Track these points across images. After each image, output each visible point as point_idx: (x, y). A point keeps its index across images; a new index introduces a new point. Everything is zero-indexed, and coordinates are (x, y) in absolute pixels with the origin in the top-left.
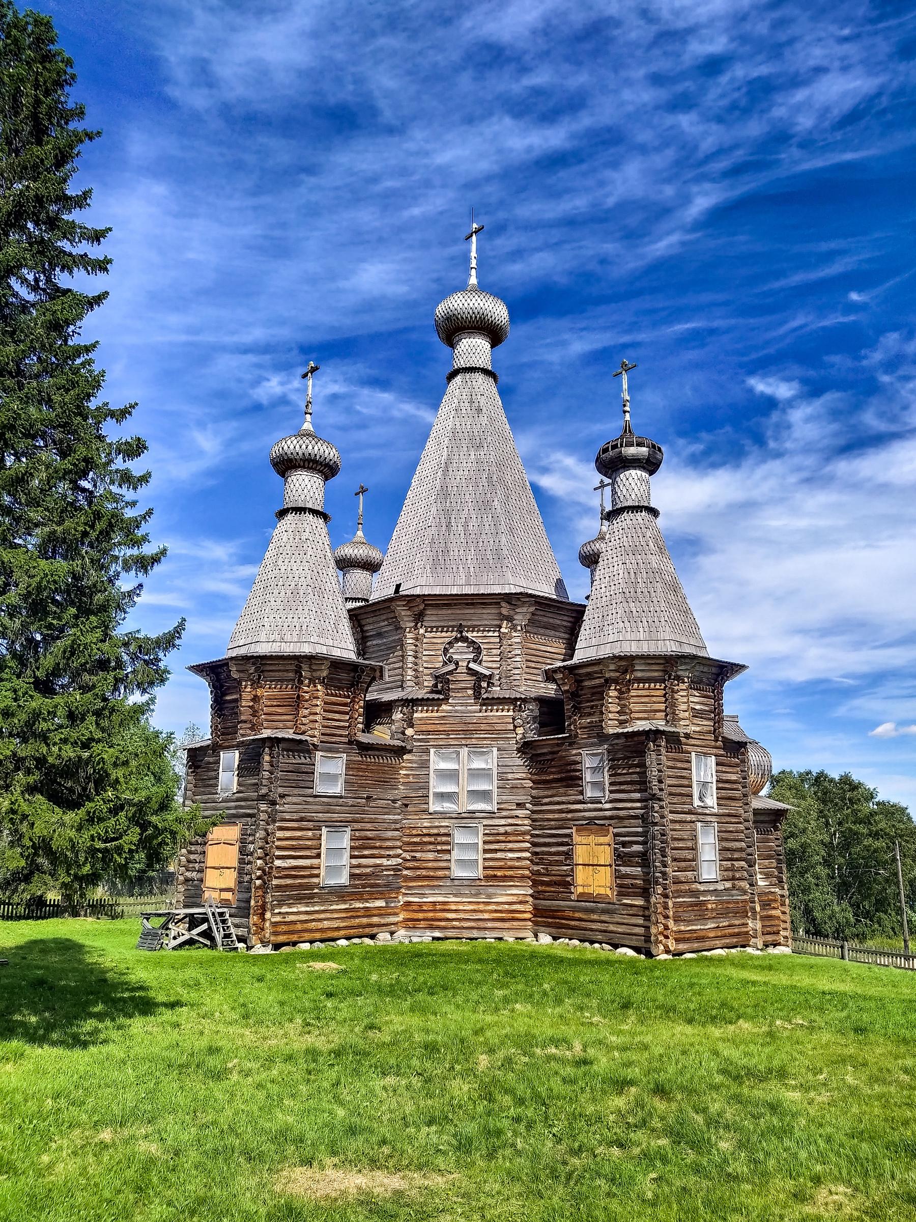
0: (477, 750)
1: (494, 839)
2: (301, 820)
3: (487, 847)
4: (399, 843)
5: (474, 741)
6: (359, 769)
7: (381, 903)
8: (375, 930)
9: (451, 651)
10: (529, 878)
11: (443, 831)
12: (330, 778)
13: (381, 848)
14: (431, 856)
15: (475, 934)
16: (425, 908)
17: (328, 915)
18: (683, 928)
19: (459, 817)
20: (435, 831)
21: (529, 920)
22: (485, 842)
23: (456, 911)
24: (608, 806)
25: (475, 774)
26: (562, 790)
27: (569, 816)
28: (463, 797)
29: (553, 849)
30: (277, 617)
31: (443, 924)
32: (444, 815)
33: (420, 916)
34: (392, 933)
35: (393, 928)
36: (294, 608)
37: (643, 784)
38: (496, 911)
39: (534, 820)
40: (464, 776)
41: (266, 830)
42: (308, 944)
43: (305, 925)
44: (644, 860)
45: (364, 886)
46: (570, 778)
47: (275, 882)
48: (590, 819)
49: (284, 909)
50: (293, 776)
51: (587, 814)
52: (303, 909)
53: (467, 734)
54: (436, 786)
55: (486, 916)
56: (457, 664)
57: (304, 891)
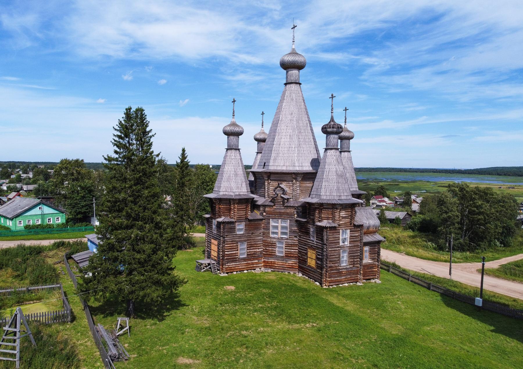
0: (283, 219)
1: (288, 245)
7: (257, 261)
12: (240, 230)
14: (270, 249)
15: (282, 271)
19: (278, 239)
25: (283, 228)
28: (279, 233)
32: (274, 238)
37: (322, 240)
40: (280, 228)
44: (321, 260)
46: (307, 233)
50: (230, 230)
53: (280, 216)
54: (271, 230)
56: (278, 195)
57: (233, 259)
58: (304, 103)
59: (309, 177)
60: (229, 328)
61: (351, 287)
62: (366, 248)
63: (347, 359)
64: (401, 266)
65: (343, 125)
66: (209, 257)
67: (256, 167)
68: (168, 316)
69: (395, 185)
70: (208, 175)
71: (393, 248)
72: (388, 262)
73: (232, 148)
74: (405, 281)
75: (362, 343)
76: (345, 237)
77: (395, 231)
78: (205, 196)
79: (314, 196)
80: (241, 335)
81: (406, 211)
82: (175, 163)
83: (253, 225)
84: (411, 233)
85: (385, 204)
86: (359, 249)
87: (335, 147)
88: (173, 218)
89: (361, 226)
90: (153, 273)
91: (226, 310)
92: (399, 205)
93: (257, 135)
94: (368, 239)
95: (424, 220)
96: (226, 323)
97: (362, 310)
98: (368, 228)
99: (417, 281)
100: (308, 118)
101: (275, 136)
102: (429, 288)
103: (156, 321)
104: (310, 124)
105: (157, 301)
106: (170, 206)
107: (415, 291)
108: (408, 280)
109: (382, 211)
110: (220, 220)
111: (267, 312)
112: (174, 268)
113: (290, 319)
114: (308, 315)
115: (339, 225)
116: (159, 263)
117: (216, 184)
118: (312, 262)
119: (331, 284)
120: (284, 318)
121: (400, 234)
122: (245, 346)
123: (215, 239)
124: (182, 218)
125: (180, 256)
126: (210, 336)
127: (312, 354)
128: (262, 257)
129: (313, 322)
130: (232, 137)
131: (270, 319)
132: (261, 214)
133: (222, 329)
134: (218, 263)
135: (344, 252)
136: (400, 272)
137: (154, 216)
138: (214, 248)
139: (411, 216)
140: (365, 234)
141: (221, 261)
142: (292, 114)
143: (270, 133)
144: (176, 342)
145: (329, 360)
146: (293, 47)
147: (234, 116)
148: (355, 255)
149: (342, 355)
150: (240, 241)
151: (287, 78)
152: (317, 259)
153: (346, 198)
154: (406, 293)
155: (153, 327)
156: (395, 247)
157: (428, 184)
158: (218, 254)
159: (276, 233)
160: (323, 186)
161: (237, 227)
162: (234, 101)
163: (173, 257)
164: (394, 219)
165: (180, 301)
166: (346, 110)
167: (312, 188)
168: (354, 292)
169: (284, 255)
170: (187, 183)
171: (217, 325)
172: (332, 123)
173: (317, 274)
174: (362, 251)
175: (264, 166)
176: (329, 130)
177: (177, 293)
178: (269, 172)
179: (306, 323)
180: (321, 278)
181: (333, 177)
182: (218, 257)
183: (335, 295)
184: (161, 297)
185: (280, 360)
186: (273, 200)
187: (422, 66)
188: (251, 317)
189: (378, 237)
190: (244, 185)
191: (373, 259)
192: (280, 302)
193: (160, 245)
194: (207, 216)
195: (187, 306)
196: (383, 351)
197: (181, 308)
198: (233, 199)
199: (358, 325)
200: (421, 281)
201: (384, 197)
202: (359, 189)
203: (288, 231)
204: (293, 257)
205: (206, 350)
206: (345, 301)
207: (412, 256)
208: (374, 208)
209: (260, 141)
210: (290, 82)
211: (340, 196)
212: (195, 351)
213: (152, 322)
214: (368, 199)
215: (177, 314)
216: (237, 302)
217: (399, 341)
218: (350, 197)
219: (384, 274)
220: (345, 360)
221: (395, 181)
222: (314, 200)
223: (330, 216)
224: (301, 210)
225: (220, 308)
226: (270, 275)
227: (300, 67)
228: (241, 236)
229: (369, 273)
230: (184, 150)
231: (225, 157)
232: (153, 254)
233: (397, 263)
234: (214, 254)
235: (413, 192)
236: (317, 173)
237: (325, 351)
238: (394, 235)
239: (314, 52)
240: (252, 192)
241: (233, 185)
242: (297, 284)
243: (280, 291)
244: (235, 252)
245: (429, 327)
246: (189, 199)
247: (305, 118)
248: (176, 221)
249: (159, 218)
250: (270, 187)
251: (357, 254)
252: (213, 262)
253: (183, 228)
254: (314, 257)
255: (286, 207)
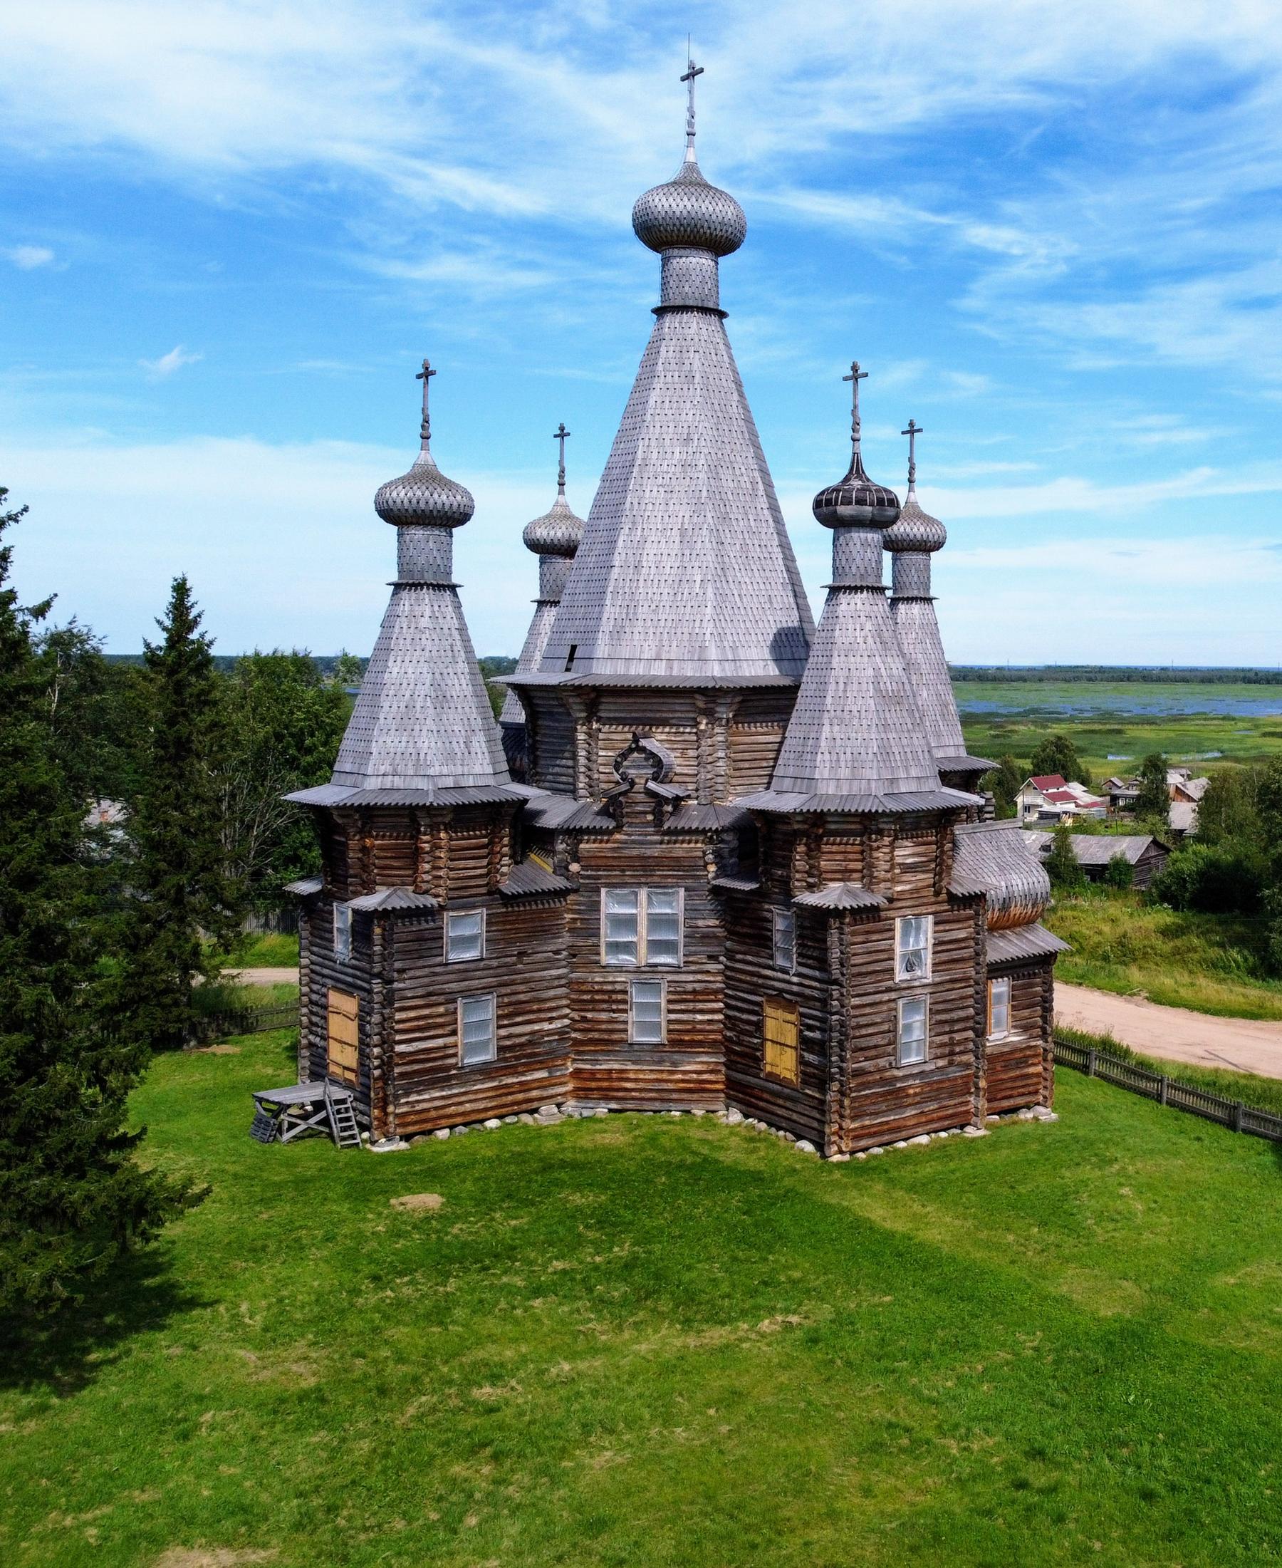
1: (680, 996)
2: (430, 994)
3: (671, 1007)
4: (565, 1002)
5: (656, 879)
6: (504, 923)
8: (535, 1105)
9: (625, 763)
10: (722, 1043)
11: (618, 987)
12: (468, 941)
13: (539, 1011)
14: (604, 1016)
15: (657, 1105)
16: (598, 1076)
17: (472, 1097)
18: (867, 1123)
19: (638, 970)
20: (610, 987)
21: (722, 1091)
22: (669, 1002)
23: (636, 1080)
24: (795, 979)
25: (657, 922)
26: (754, 949)
27: (760, 981)
28: (643, 948)
29: (745, 1016)
30: (389, 740)
31: (620, 1094)
32: (620, 969)
33: (593, 1085)
34: (559, 1105)
35: (560, 1099)
36: (409, 728)
37: (823, 964)
38: (683, 1081)
39: (728, 977)
41: (382, 1014)
42: (447, 1130)
43: (442, 1112)
44: (820, 1047)
45: (517, 1058)
46: (761, 940)
47: (397, 1070)
48: (782, 991)
49: (413, 1098)
50: (415, 946)
51: (777, 984)
52: (438, 1094)
53: (645, 872)
54: (607, 935)
55: (671, 1086)
56: (632, 783)
57: (436, 1072)
58: (741, 395)
59: (768, 704)
60: (415, 1379)
61: (943, 1147)
62: (1000, 987)
63: (928, 1442)
64: (1135, 1049)
65: (901, 493)
66: (319, 1071)
67: (535, 666)
68: (112, 1362)
69: (1110, 730)
70: (304, 705)
71: (1102, 978)
72: (1083, 1037)
73: (423, 580)
74: (1146, 1106)
75: (985, 1369)
76: (915, 943)
77: (1112, 911)
78: (291, 797)
79: (787, 783)
80: (470, 1405)
81: (1151, 832)
82: (140, 650)
83: (521, 918)
84: (1164, 916)
85: (1071, 807)
86: (971, 991)
87: (870, 582)
88: (134, 903)
89: (976, 900)
90: (23, 1169)
91: (399, 1304)
92: (1124, 809)
93: (535, 524)
94: (1005, 948)
95: (1213, 864)
96: (401, 1360)
97: (983, 1235)
98: (1006, 905)
99: (1189, 1101)
100: (760, 458)
101: (614, 530)
102: (1232, 1125)
103: (42, 1393)
104: (769, 485)
105: (45, 1302)
106: (122, 848)
107: (1183, 1141)
108: (1158, 1098)
109: (1063, 833)
110: (367, 902)
111: (590, 1290)
112: (139, 1137)
113: (693, 1307)
114: (765, 1284)
115: (891, 900)
116: (58, 1121)
117: (349, 742)
118: (782, 1061)
119: (863, 1143)
120: (665, 1305)
121: (1127, 925)
122: (488, 1451)
123: (347, 989)
124: (178, 901)
125: (169, 1078)
126: (321, 1427)
127: (783, 1444)
128: (565, 1057)
129: (787, 1311)
130: (417, 533)
131: (601, 1319)
132: (562, 869)
133: (383, 1391)
134: (364, 1097)
135: (912, 1006)
136: (1129, 1071)
137: (22, 899)
138: (343, 1028)
139: (1168, 851)
140: (992, 929)
141: (378, 1085)
142: (688, 439)
143: (594, 518)
144: (154, 1477)
145: (854, 1460)
146: (691, 158)
147: (426, 437)
148: (955, 1015)
149: (907, 1430)
150: (465, 993)
151: (664, 284)
152: (805, 1043)
153: (919, 789)
154: (1152, 1151)
155: (31, 1425)
156: (1112, 975)
157: (1228, 725)
158: (363, 1055)
159: (628, 948)
160: (823, 743)
161: (450, 932)
162: (427, 374)
163: (128, 1087)
164: (1104, 867)
165: (174, 1286)
166: (912, 431)
167: (779, 751)
168: (952, 1165)
169: (662, 1037)
170: (201, 742)
171: (357, 1374)
172: (857, 483)
173: (799, 1107)
174: (981, 1002)
175: (571, 659)
176: (843, 510)
177: (155, 1252)
178: (594, 688)
179: (760, 1319)
180: (822, 1122)
181: (863, 703)
182: (363, 1068)
183: (879, 1187)
184: (66, 1281)
185: (645, 1489)
186: (614, 807)
187: (1184, 273)
188: (517, 1322)
189: (1042, 940)
190: (479, 744)
191: (1025, 1029)
192: (645, 1239)
193: (61, 1036)
194: (306, 887)
195: (205, 1305)
196: (1065, 1389)
197: (174, 1319)
198: (429, 810)
199: (970, 1299)
200: (1206, 1099)
201: (1067, 780)
202: (971, 750)
203: (679, 936)
204: (700, 1043)
205: (300, 1495)
206: (916, 1207)
207: (1173, 1004)
208: (1027, 827)
209: (545, 550)
210: (679, 302)
211: (893, 781)
212: (244, 1509)
213: (27, 1401)
214: (1006, 787)
215: (161, 1349)
216: (451, 1260)
217: (1128, 1342)
218: (934, 784)
219: (1071, 1086)
220: (918, 1448)
221: (1107, 716)
222: (787, 803)
223: (853, 865)
224: (735, 844)
225: (370, 1298)
226: (603, 1129)
227: (720, 243)
228: (465, 971)
229: (1009, 1083)
230: (181, 590)
231: (388, 622)
232: (20, 1082)
233: (1116, 1037)
234: (343, 1056)
235: (1174, 758)
236: (797, 687)
237: (839, 1422)
238: (1106, 928)
239: (767, 185)
240: (518, 775)
241: (427, 743)
242: (721, 1156)
243: (629, 1190)
244: (440, 1042)
245: (1233, 1273)
246: (216, 817)
247: (744, 460)
248: (147, 919)
249: (49, 909)
250: (599, 750)
251: (962, 1014)
252: (338, 1093)
253: (188, 947)
254: (791, 1037)
255: (669, 832)
